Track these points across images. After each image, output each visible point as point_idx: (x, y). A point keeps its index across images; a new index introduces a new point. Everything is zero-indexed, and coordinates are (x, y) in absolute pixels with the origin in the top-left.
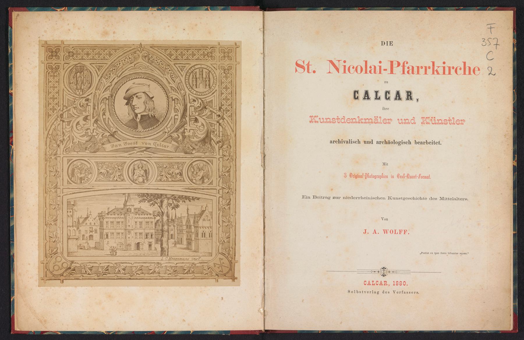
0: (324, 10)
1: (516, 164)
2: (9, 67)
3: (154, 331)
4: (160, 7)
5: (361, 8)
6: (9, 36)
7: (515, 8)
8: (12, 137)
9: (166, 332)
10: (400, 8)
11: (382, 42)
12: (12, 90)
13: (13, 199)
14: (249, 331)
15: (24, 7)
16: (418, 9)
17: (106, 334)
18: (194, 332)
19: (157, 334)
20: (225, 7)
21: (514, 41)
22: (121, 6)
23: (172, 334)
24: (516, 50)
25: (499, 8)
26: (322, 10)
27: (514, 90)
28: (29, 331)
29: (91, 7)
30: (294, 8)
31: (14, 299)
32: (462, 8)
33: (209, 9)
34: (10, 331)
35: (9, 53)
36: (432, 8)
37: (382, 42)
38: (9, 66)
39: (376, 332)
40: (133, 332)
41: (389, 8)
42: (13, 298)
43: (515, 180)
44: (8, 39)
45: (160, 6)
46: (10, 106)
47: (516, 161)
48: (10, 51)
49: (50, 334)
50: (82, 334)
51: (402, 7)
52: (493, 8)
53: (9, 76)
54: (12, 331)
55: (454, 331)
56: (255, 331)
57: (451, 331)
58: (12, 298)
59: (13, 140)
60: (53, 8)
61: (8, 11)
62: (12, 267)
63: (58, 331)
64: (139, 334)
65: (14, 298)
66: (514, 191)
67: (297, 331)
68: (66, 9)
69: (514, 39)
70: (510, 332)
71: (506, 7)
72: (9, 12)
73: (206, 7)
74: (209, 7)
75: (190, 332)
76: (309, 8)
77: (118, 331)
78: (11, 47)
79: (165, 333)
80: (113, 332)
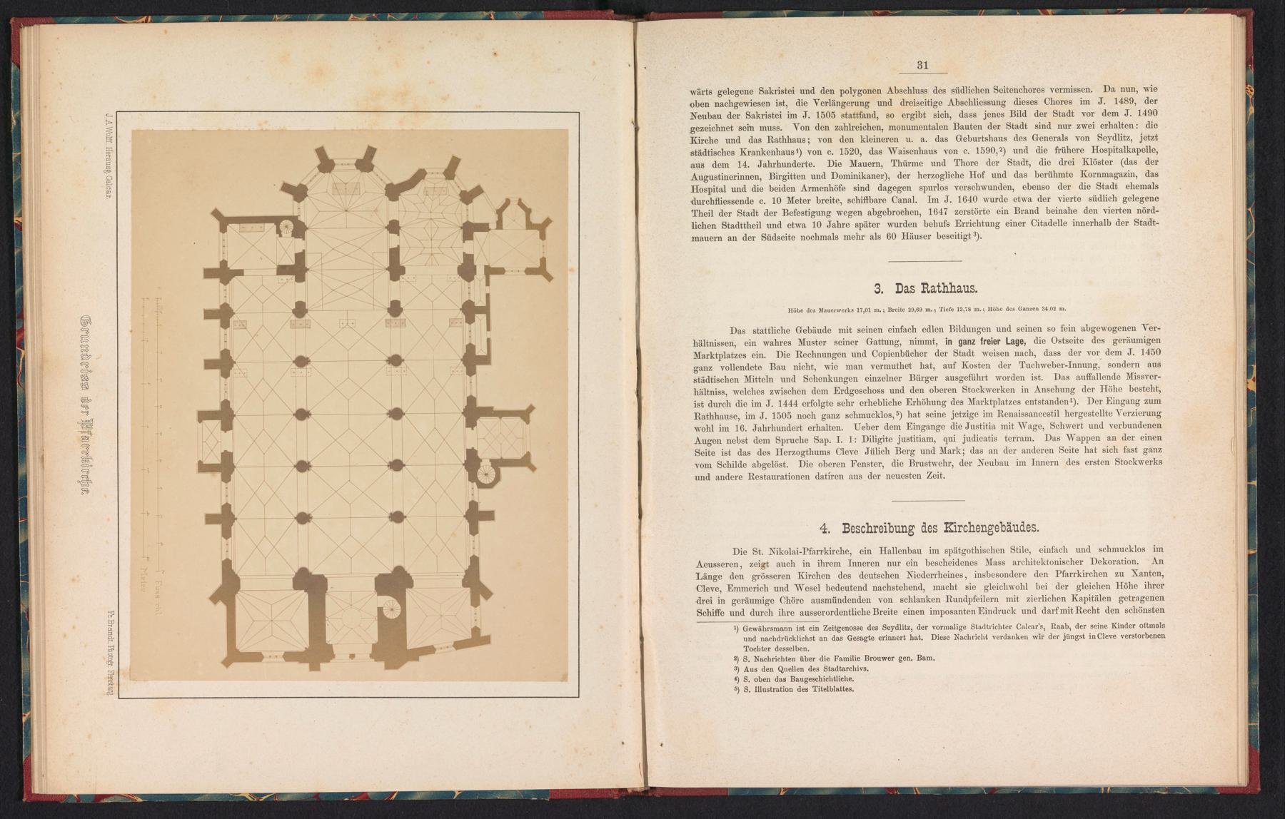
1: (1253, 387)
3: (366, 792)
4: (374, 15)
5: (879, 12)
6: (12, 87)
7: (1251, 9)
8: (22, 330)
9: (395, 794)
10: (975, 11)
11: (1105, 86)
12: (20, 215)
13: (25, 477)
14: (595, 790)
15: (48, 16)
17: (250, 799)
18: (464, 793)
19: (372, 801)
20: (530, 12)
21: (1249, 91)
23: (410, 799)
24: (1253, 111)
27: (1250, 209)
28: (67, 795)
30: (718, 13)
33: (492, 17)
34: (22, 797)
35: (13, 128)
37: (1105, 86)
38: (13, 158)
39: (919, 793)
40: (317, 795)
41: (947, 11)
44: (10, 95)
45: (374, 12)
47: (1253, 380)
48: (14, 122)
49: (116, 801)
50: (195, 800)
51: (980, 9)
53: (14, 181)
54: (25, 794)
55: (1106, 788)
56: (610, 790)
58: (25, 716)
59: (23, 336)
61: (10, 25)
62: (25, 642)
63: (135, 795)
64: (332, 799)
65: (30, 715)
72: (12, 29)
73: (484, 12)
75: (453, 793)
77: (280, 794)
78: (18, 113)
79: (394, 796)
80: (268, 796)
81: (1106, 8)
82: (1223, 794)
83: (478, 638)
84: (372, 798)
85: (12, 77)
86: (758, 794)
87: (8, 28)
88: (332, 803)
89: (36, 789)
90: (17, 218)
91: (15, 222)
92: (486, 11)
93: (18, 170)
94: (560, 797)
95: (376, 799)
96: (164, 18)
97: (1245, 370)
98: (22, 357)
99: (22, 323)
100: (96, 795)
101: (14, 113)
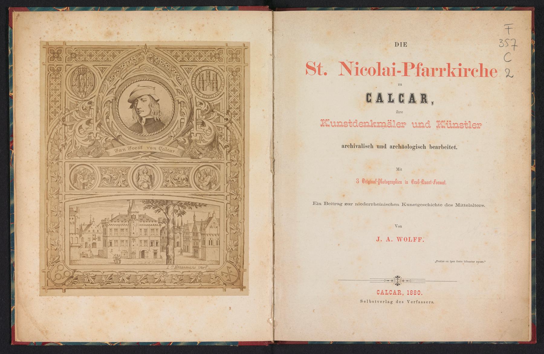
1: (534, 169)
4: (165, 7)
5: (374, 8)
6: (9, 37)
7: (534, 7)
8: (12, 142)
9: (172, 343)
12: (12, 92)
16: (433, 9)
17: (109, 345)
19: (162, 346)
20: (233, 7)
21: (533, 42)
23: (178, 345)
26: (333, 10)
27: (533, 93)
30: (305, 8)
32: (479, 7)
33: (216, 9)
34: (10, 342)
35: (9, 54)
36: (447, 8)
38: (9, 67)
39: (390, 343)
40: (138, 343)
42: (13, 308)
45: (165, 6)
47: (534, 166)
48: (10, 53)
49: (51, 345)
51: (417, 7)
52: (511, 8)
53: (9, 77)
54: (12, 342)
55: (470, 342)
57: (468, 342)
61: (8, 10)
62: (13, 276)
63: (60, 342)
65: (14, 308)
68: (68, 9)
69: (533, 40)
72: (9, 12)
74: (216, 7)
75: (197, 343)
76: (319, 8)
78: (11, 48)
81: (471, 7)
82: (520, 344)
83: (403, 294)
84: (162, 345)
85: (9, 33)
86: (321, 343)
87: (7, 12)
88: (145, 346)
89: (17, 339)
90: (11, 94)
91: (10, 95)
92: (214, 6)
93: (11, 73)
94: (243, 345)
95: (163, 345)
96: (75, 8)
97: (531, 162)
98: (12, 153)
99: (12, 138)
100: (43, 342)
101: (10, 48)
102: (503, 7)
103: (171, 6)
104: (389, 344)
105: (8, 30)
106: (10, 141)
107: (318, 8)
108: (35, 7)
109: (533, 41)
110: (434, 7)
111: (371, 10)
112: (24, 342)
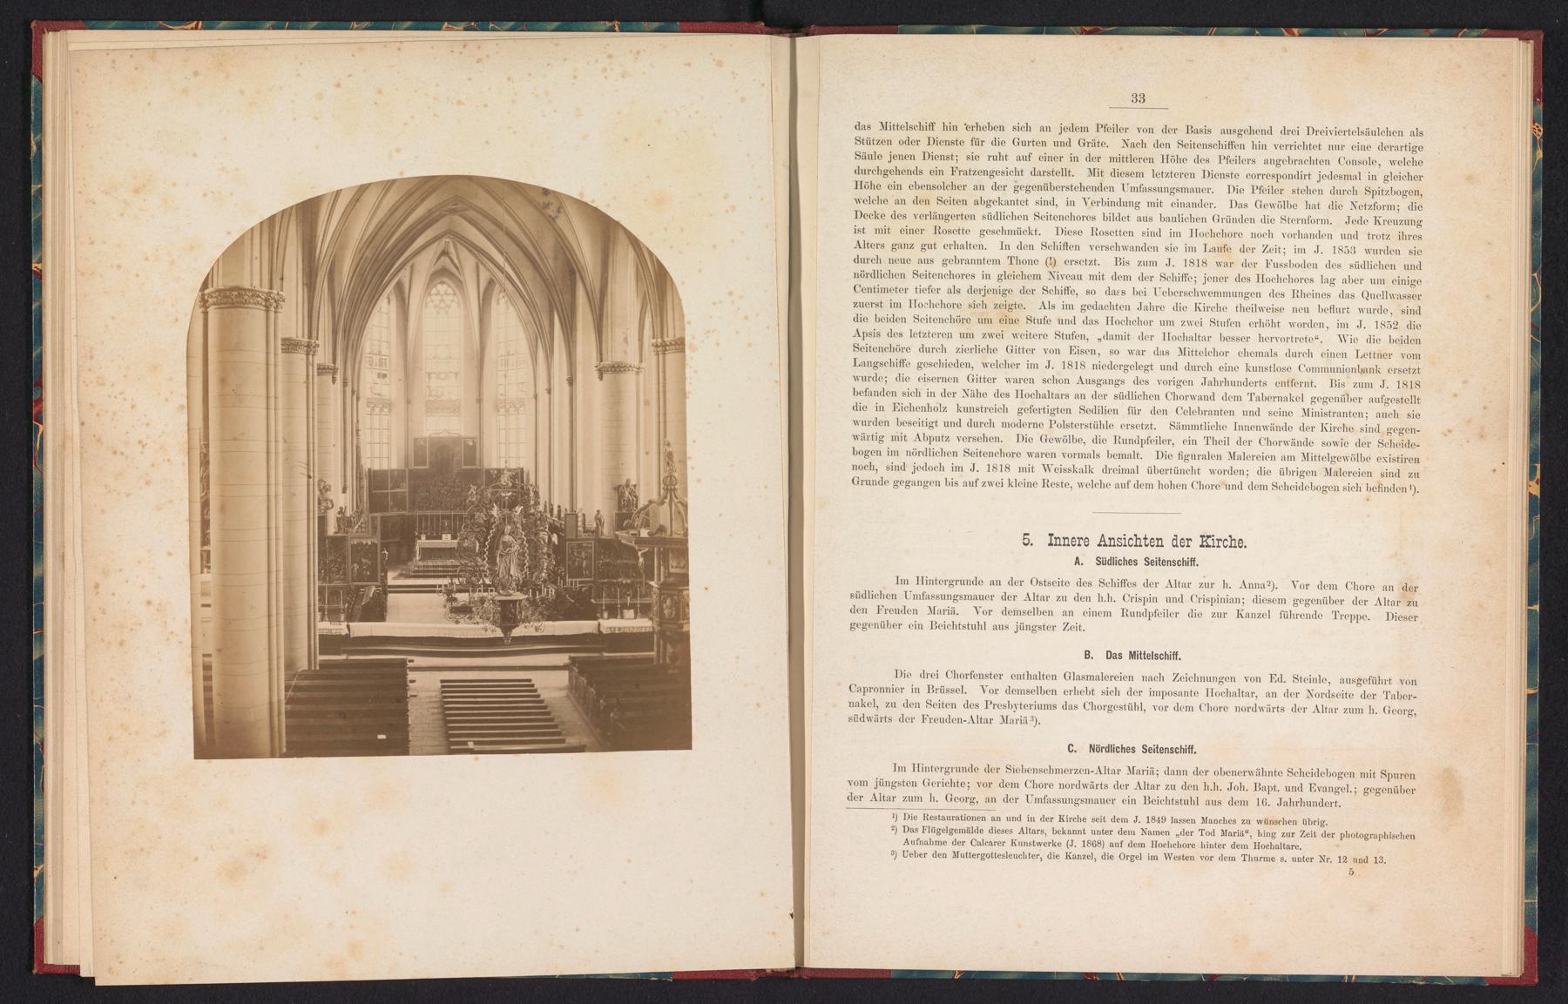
0: (979, 32)
2: (32, 194)
5: (1087, 29)
6: (32, 105)
8: (40, 400)
10: (1204, 28)
12: (40, 261)
16: (1257, 32)
20: (663, 24)
21: (1537, 131)
22: (359, 20)
25: (1490, 32)
26: (972, 33)
27: (1535, 275)
29: (271, 22)
31: (43, 873)
32: (1385, 30)
33: (617, 28)
35: (32, 154)
36: (1295, 30)
38: (33, 190)
42: (39, 868)
43: (1535, 539)
44: (30, 114)
45: (472, 21)
46: (36, 356)
47: (1537, 483)
48: (34, 148)
51: (1211, 26)
52: (1476, 32)
53: (33, 219)
54: (35, 966)
55: (1350, 977)
57: (1343, 977)
60: (161, 22)
61: (31, 30)
62: (38, 779)
65: (43, 868)
66: (1531, 571)
67: (889, 971)
68: (200, 26)
69: (1536, 124)
70: (1515, 983)
71: (1514, 29)
72: (34, 35)
73: (607, 23)
74: (616, 23)
76: (934, 27)
78: (39, 137)
85: (33, 93)
90: (37, 265)
91: (33, 268)
92: (611, 21)
98: (40, 433)
101: (34, 137)
102: (1455, 31)
103: (488, 21)
104: (1121, 980)
105: (30, 84)
106: (34, 397)
107: (930, 27)
108: (307, 21)
109: (1537, 127)
110: (1259, 26)
111: (1082, 34)
112: (69, 966)
